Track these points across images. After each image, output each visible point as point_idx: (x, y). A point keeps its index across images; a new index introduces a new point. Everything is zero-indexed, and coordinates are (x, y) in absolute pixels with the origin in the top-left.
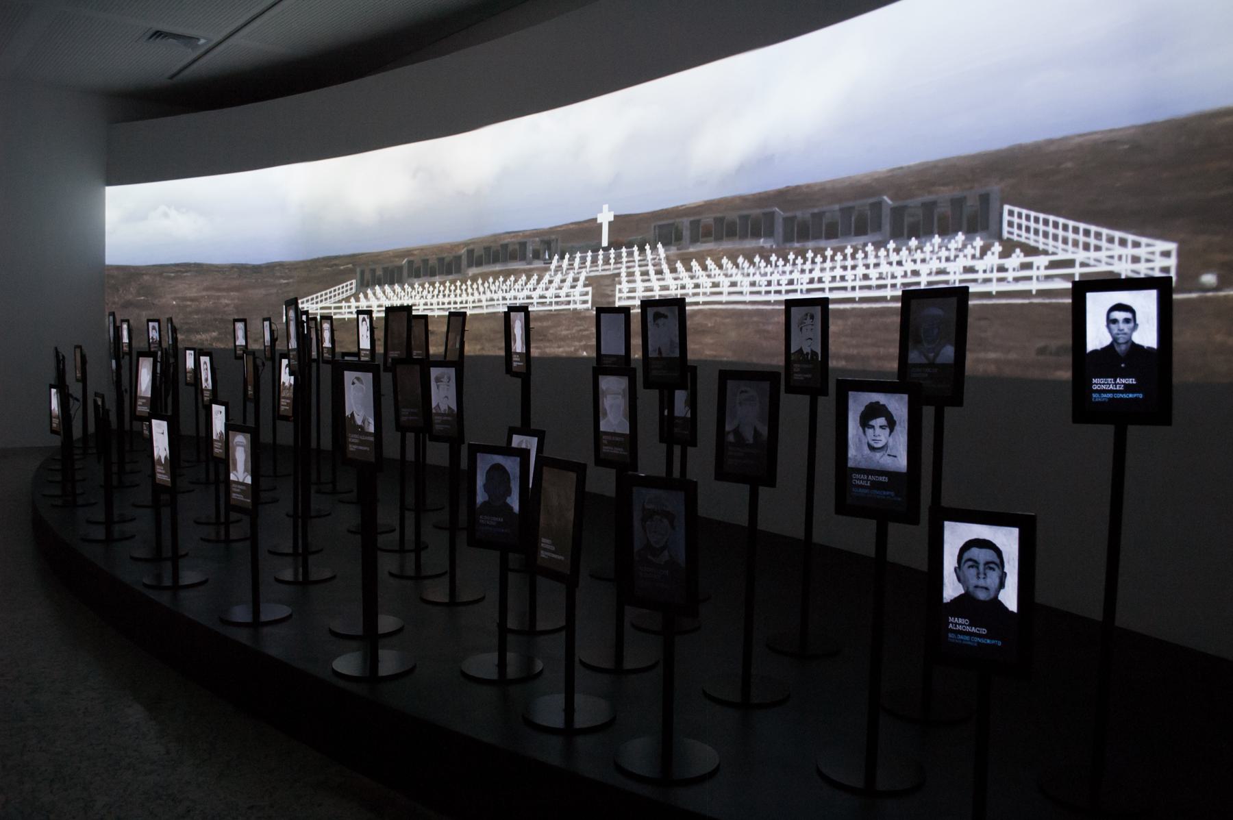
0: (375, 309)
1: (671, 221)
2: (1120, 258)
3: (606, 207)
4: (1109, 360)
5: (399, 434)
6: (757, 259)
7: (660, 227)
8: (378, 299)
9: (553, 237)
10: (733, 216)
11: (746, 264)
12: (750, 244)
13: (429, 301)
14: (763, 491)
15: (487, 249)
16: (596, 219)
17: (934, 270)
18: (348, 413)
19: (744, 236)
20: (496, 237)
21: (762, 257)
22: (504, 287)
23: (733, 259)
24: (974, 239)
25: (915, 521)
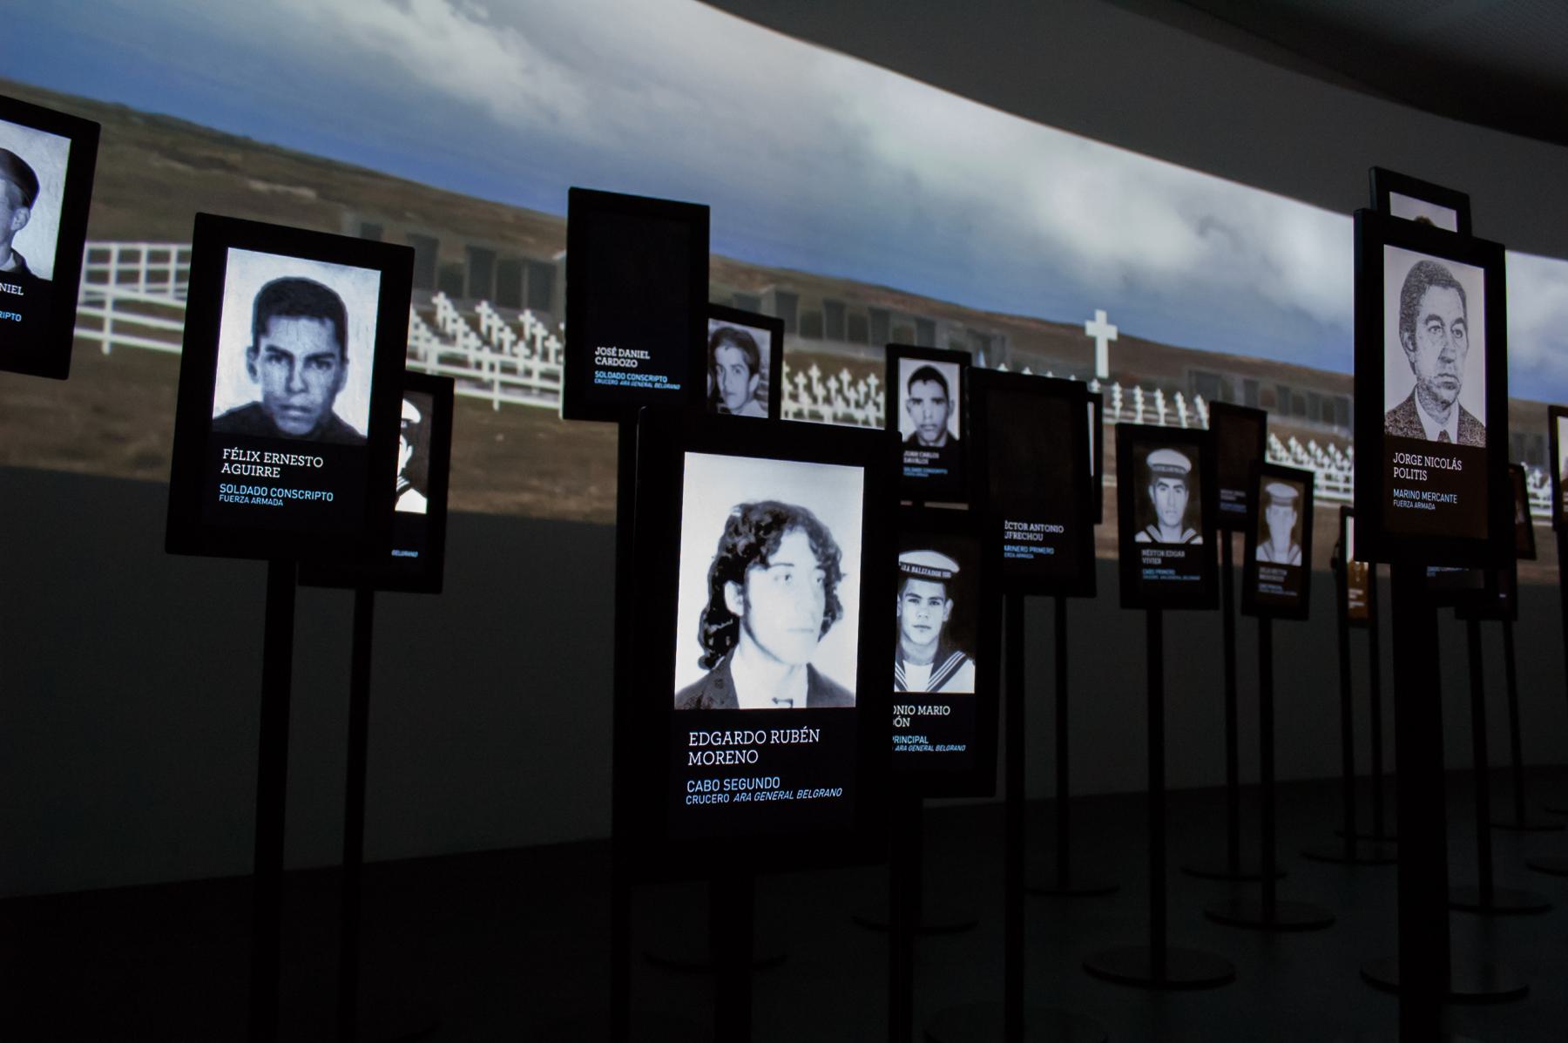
0: (1320, 481)
1: (1214, 371)
2: (492, 368)
3: (1101, 315)
4: (255, 426)
5: (1139, 617)
6: (1332, 449)
7: (1199, 374)
8: (448, 339)
9: (995, 331)
10: (1299, 389)
11: (1319, 453)
12: (1321, 428)
13: (521, 363)
14: (1072, 604)
15: (835, 307)
16: (1082, 329)
17: (840, 415)
18: (950, 604)
19: (1315, 418)
20: (854, 289)
21: (1337, 447)
22: (851, 394)
23: (1323, 445)
24: (559, 340)
25: (1216, 608)
